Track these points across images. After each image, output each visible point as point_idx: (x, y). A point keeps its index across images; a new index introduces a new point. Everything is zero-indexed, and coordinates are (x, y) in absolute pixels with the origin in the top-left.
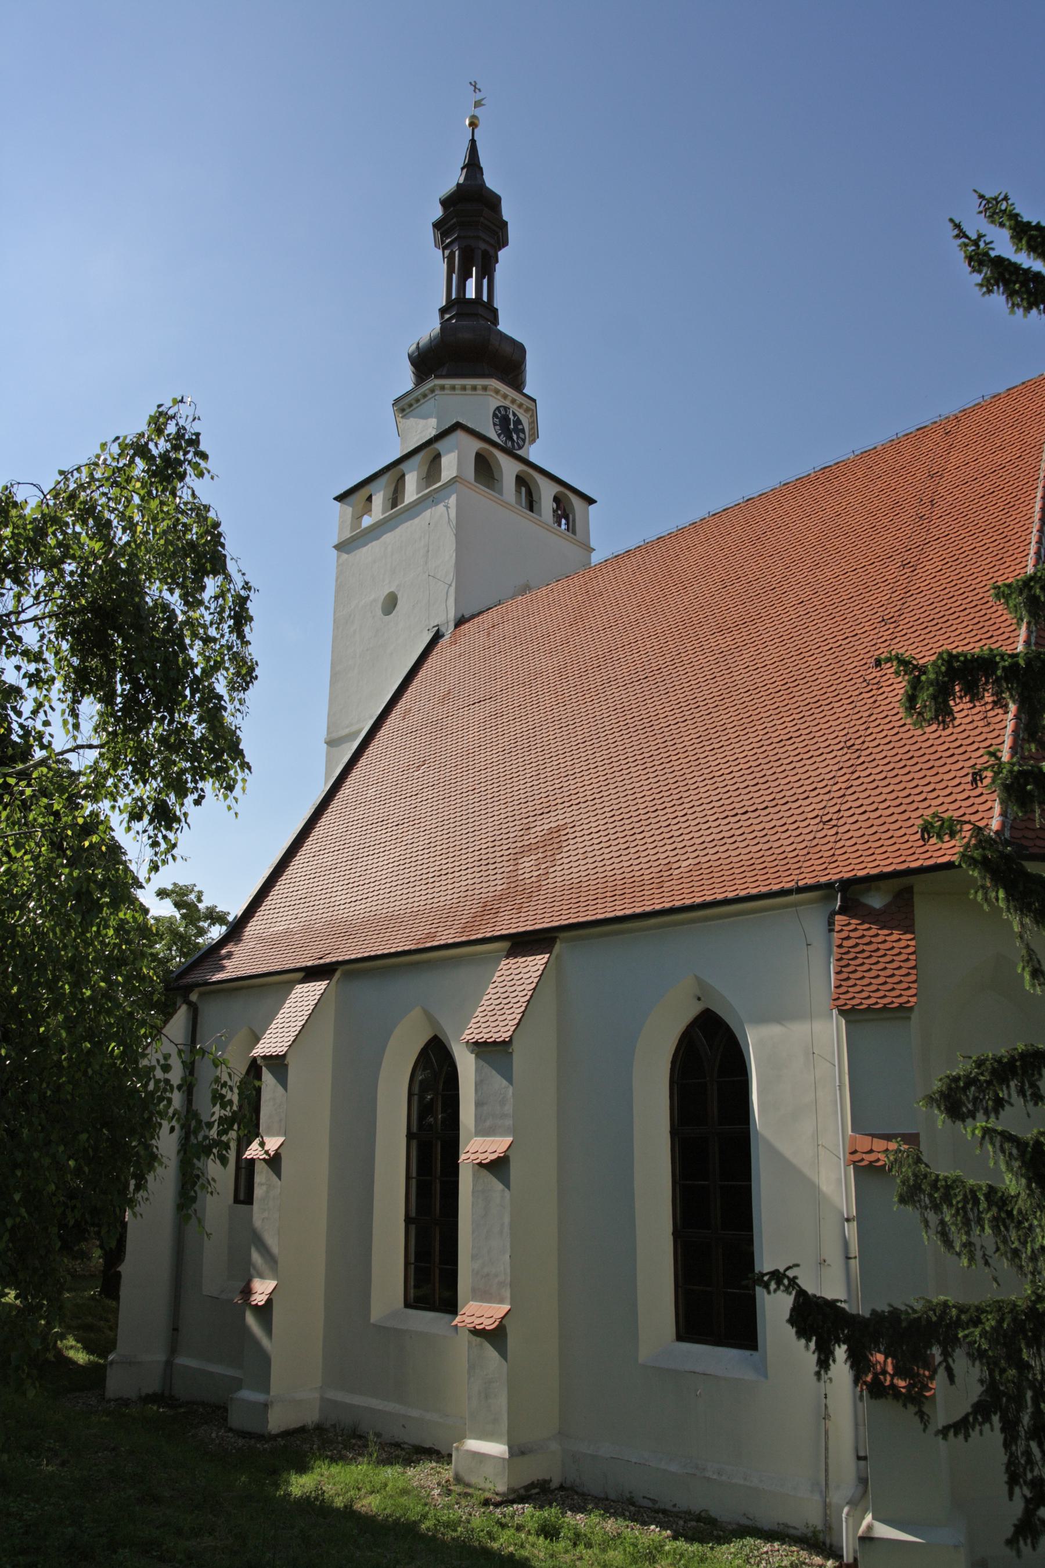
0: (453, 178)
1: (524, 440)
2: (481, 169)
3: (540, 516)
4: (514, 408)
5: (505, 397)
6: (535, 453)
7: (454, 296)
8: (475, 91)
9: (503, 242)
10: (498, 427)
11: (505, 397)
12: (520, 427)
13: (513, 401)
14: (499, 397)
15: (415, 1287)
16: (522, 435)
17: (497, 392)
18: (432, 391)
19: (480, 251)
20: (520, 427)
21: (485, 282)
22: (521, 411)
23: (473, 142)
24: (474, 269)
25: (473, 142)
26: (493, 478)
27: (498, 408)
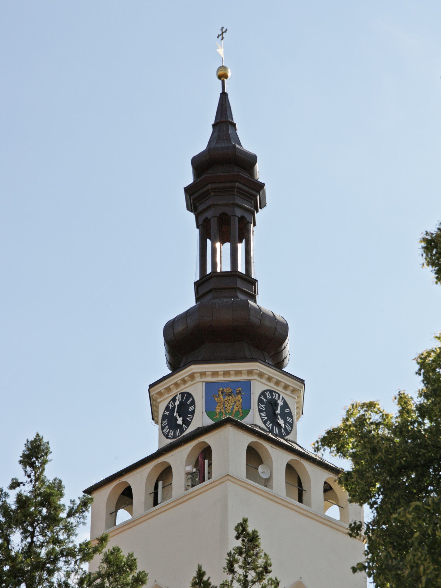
2: (234, 125)
4: (279, 389)
5: (269, 379)
8: (226, 31)
9: (188, 190)
10: (264, 414)
11: (269, 379)
12: (287, 411)
13: (278, 383)
14: (264, 381)
16: (289, 419)
17: (261, 375)
18: (192, 376)
19: (237, 219)
20: (287, 411)
21: (241, 247)
22: (288, 392)
23: (224, 96)
24: (184, 400)
25: (224, 96)
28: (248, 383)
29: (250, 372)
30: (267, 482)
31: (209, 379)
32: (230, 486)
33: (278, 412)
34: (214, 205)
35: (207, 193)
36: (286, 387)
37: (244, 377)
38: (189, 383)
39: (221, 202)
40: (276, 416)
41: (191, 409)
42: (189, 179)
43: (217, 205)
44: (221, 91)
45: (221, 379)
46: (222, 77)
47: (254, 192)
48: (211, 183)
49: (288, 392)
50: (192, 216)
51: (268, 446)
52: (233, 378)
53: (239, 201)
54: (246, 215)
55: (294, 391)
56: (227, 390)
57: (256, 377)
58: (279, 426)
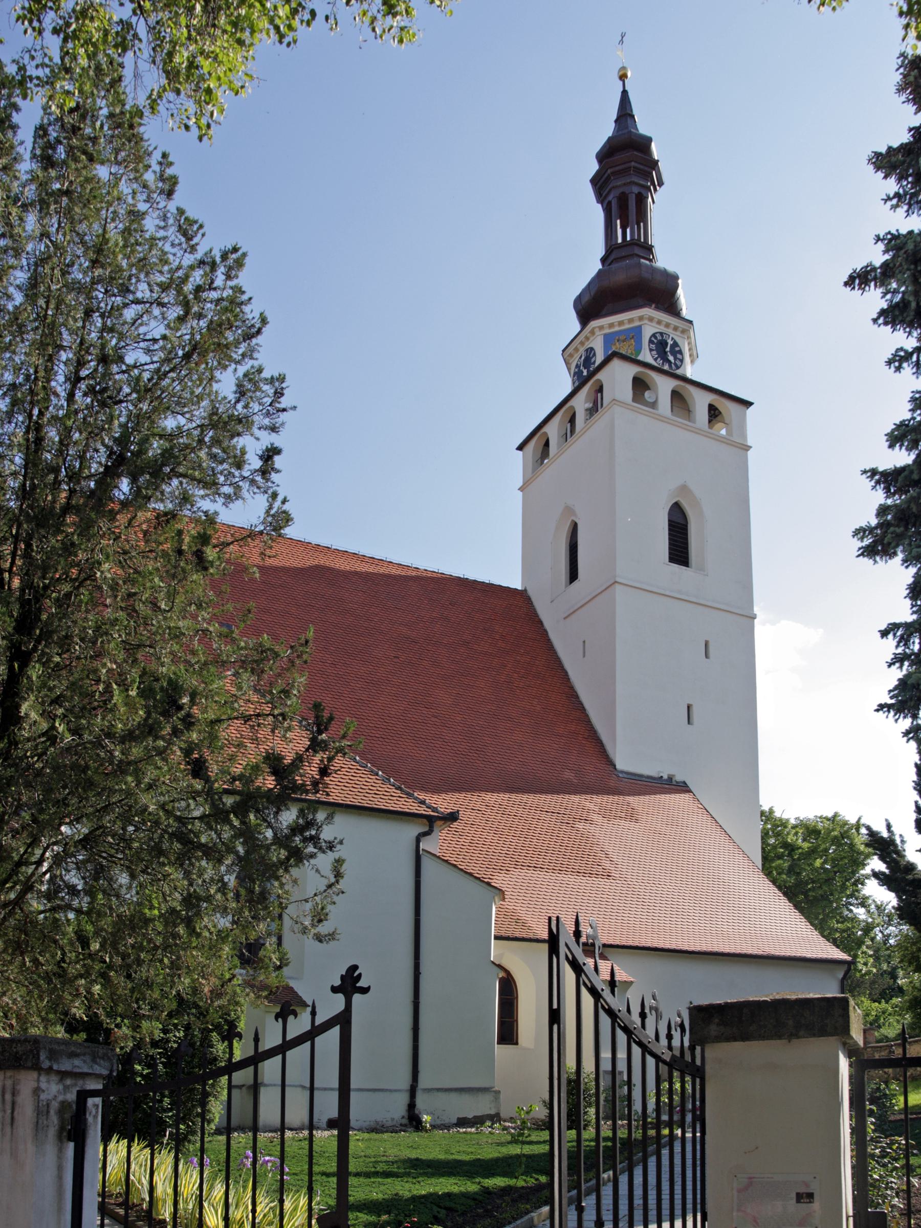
0: (607, 129)
1: (682, 361)
2: (633, 117)
3: (694, 422)
4: (669, 331)
5: (659, 322)
6: (690, 371)
7: (628, 239)
9: (594, 181)
10: (654, 353)
11: (659, 322)
12: (677, 349)
13: (667, 325)
14: (654, 324)
15: (569, 1175)
17: (651, 319)
18: (592, 332)
19: (634, 196)
20: (677, 349)
23: (625, 93)
26: (689, 411)
27: (654, 335)
28: (640, 328)
29: (641, 318)
30: (654, 405)
31: (607, 331)
32: (617, 409)
33: (668, 349)
34: (613, 187)
35: (608, 178)
36: (676, 329)
37: (637, 324)
38: (591, 339)
39: (619, 183)
40: (666, 353)
41: (593, 360)
42: (594, 167)
43: (617, 187)
44: (621, 89)
45: (617, 329)
46: (623, 77)
47: (649, 170)
48: (611, 168)
49: (678, 333)
50: (599, 206)
51: (654, 375)
52: (627, 326)
53: (635, 179)
54: (643, 191)
55: (684, 331)
56: (622, 337)
57: (646, 321)
58: (670, 362)
